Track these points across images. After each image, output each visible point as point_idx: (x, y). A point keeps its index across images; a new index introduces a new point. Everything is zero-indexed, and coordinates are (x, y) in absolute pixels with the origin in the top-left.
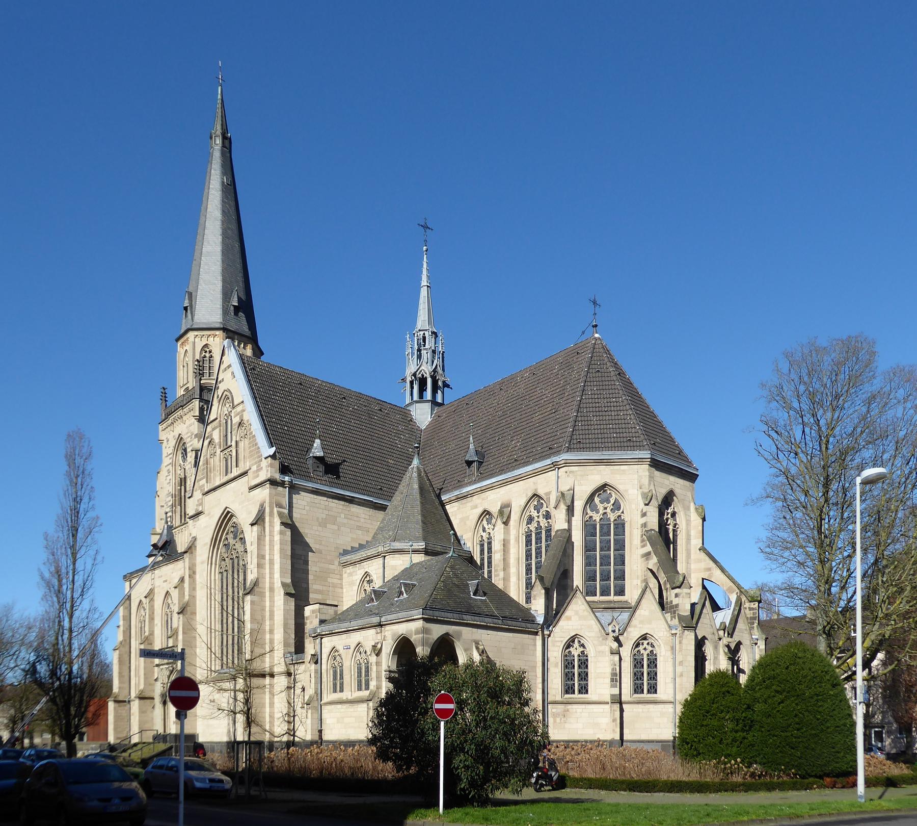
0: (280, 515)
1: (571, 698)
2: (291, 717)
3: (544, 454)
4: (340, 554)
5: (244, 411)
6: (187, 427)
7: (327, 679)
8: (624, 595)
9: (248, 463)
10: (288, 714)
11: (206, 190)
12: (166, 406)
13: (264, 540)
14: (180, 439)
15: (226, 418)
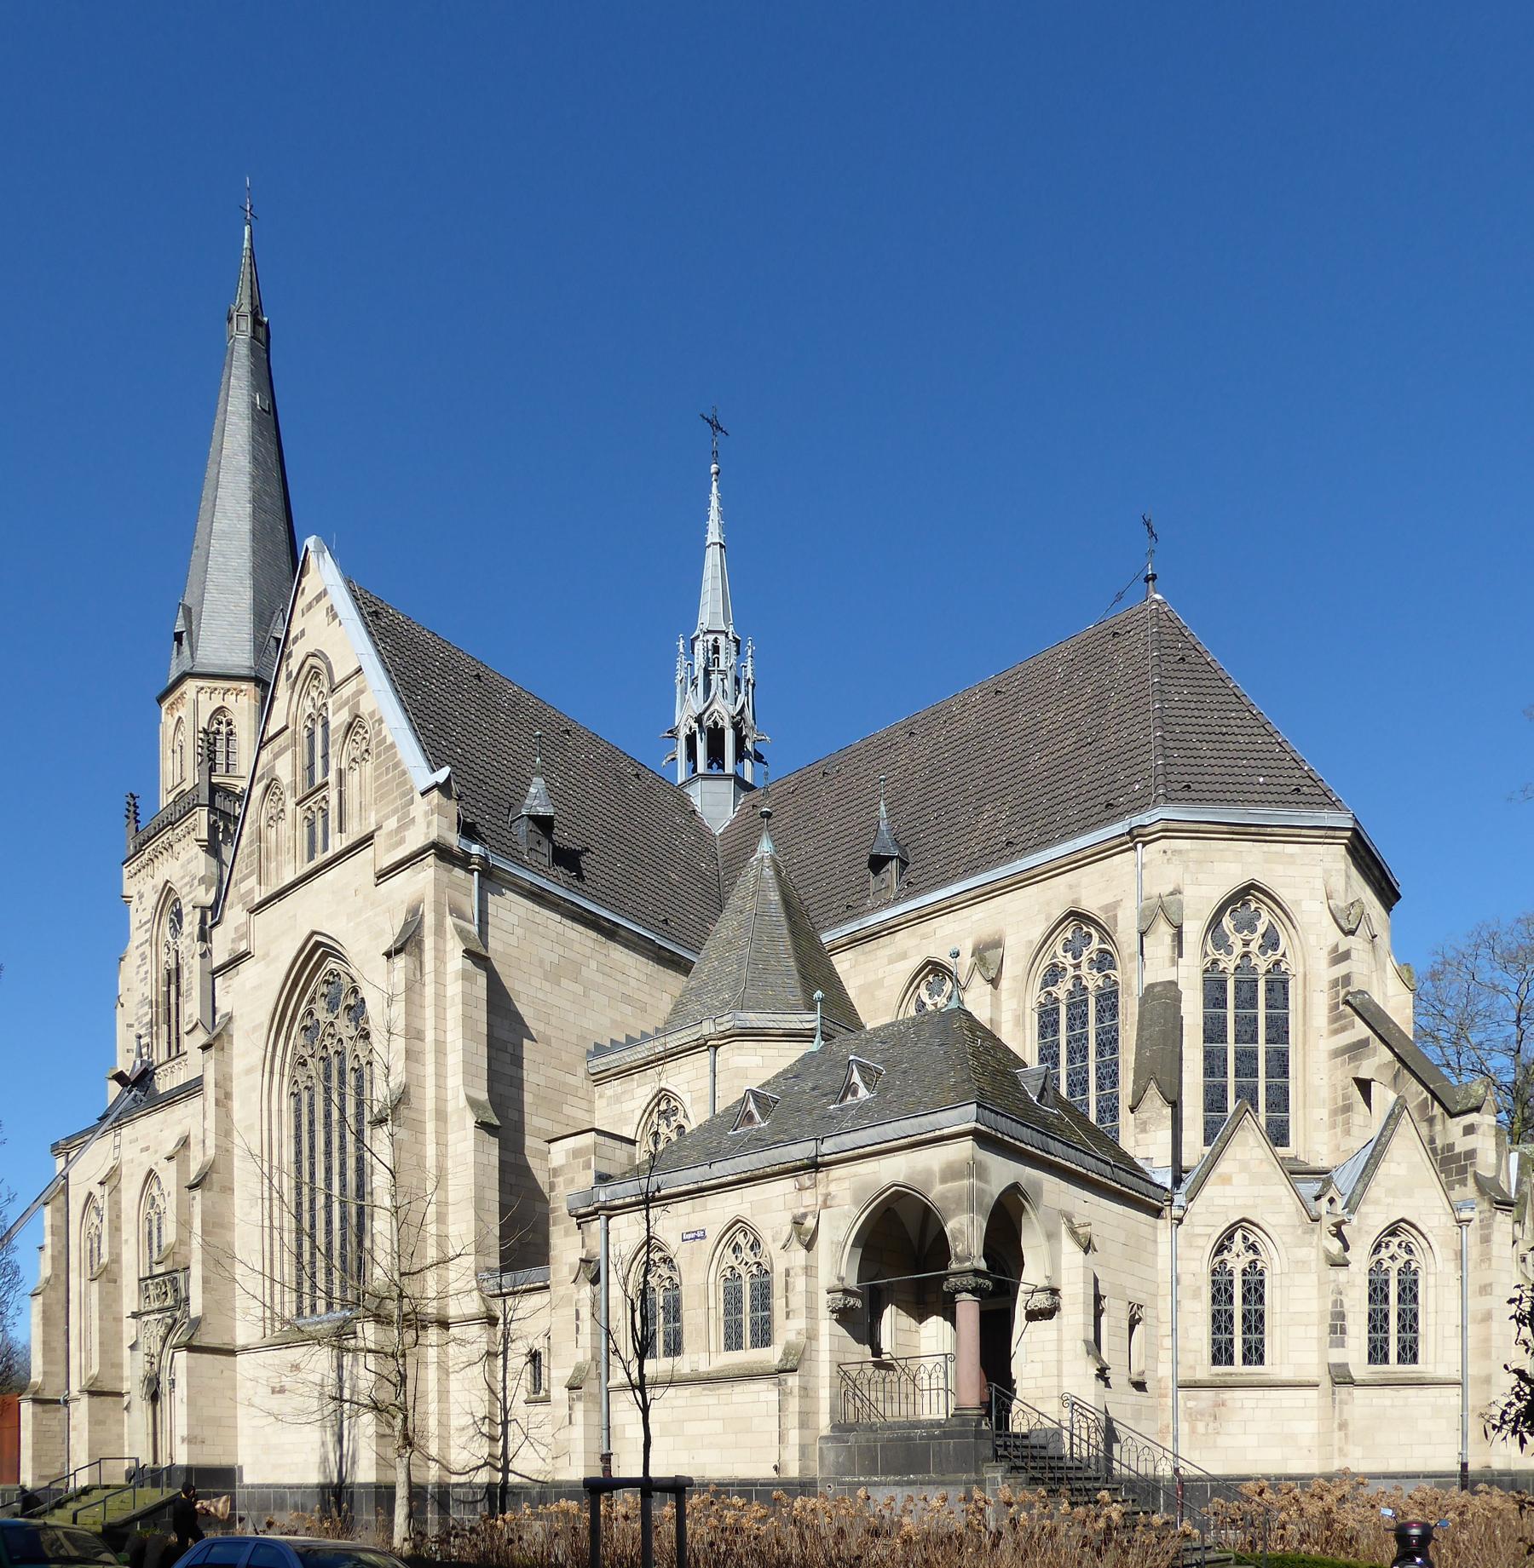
0: (462, 934)
1: (1226, 1374)
2: (498, 1425)
3: (1093, 820)
4: (588, 1052)
5: (361, 692)
6: (182, 866)
8: (1287, 1145)
9: (373, 814)
10: (489, 1418)
11: (220, 417)
12: (137, 828)
13: (422, 995)
14: (168, 890)
15: (309, 724)
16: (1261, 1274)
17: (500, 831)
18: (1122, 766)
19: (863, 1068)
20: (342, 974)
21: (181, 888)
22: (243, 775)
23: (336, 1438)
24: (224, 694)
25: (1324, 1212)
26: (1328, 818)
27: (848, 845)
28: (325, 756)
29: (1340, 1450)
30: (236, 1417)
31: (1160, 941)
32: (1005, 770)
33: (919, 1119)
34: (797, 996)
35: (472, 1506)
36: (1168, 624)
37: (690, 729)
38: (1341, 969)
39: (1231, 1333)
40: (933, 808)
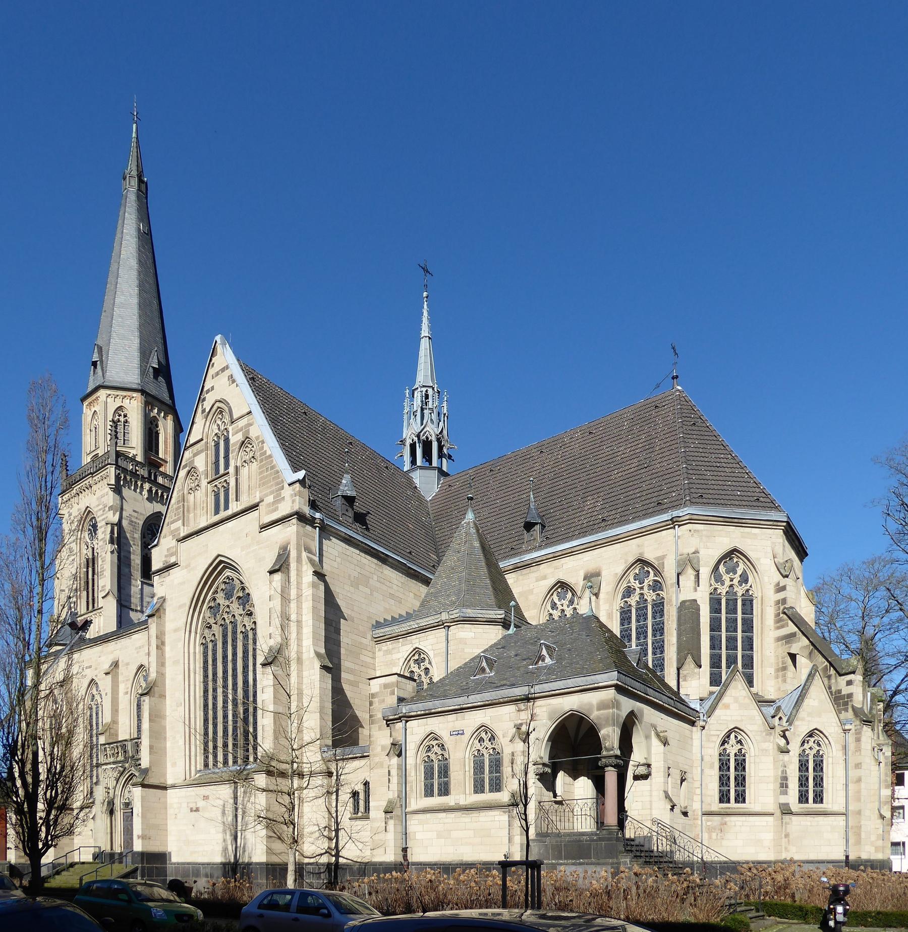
0: (311, 561)
1: (727, 808)
2: (334, 830)
3: (650, 510)
6: (98, 499)
7: (416, 778)
9: (258, 492)
10: (328, 827)
11: (118, 235)
16: (744, 756)
17: (327, 504)
18: (665, 482)
19: (548, 647)
20: (235, 579)
21: (97, 512)
22: (134, 446)
23: (233, 837)
24: (123, 399)
25: (776, 725)
26: (774, 515)
27: (508, 513)
28: (227, 457)
29: (786, 848)
30: (167, 825)
31: (688, 579)
32: (598, 478)
33: (586, 678)
34: (492, 600)
35: (318, 875)
36: (685, 403)
37: (413, 440)
38: (781, 595)
39: (729, 787)
40: (558, 496)
